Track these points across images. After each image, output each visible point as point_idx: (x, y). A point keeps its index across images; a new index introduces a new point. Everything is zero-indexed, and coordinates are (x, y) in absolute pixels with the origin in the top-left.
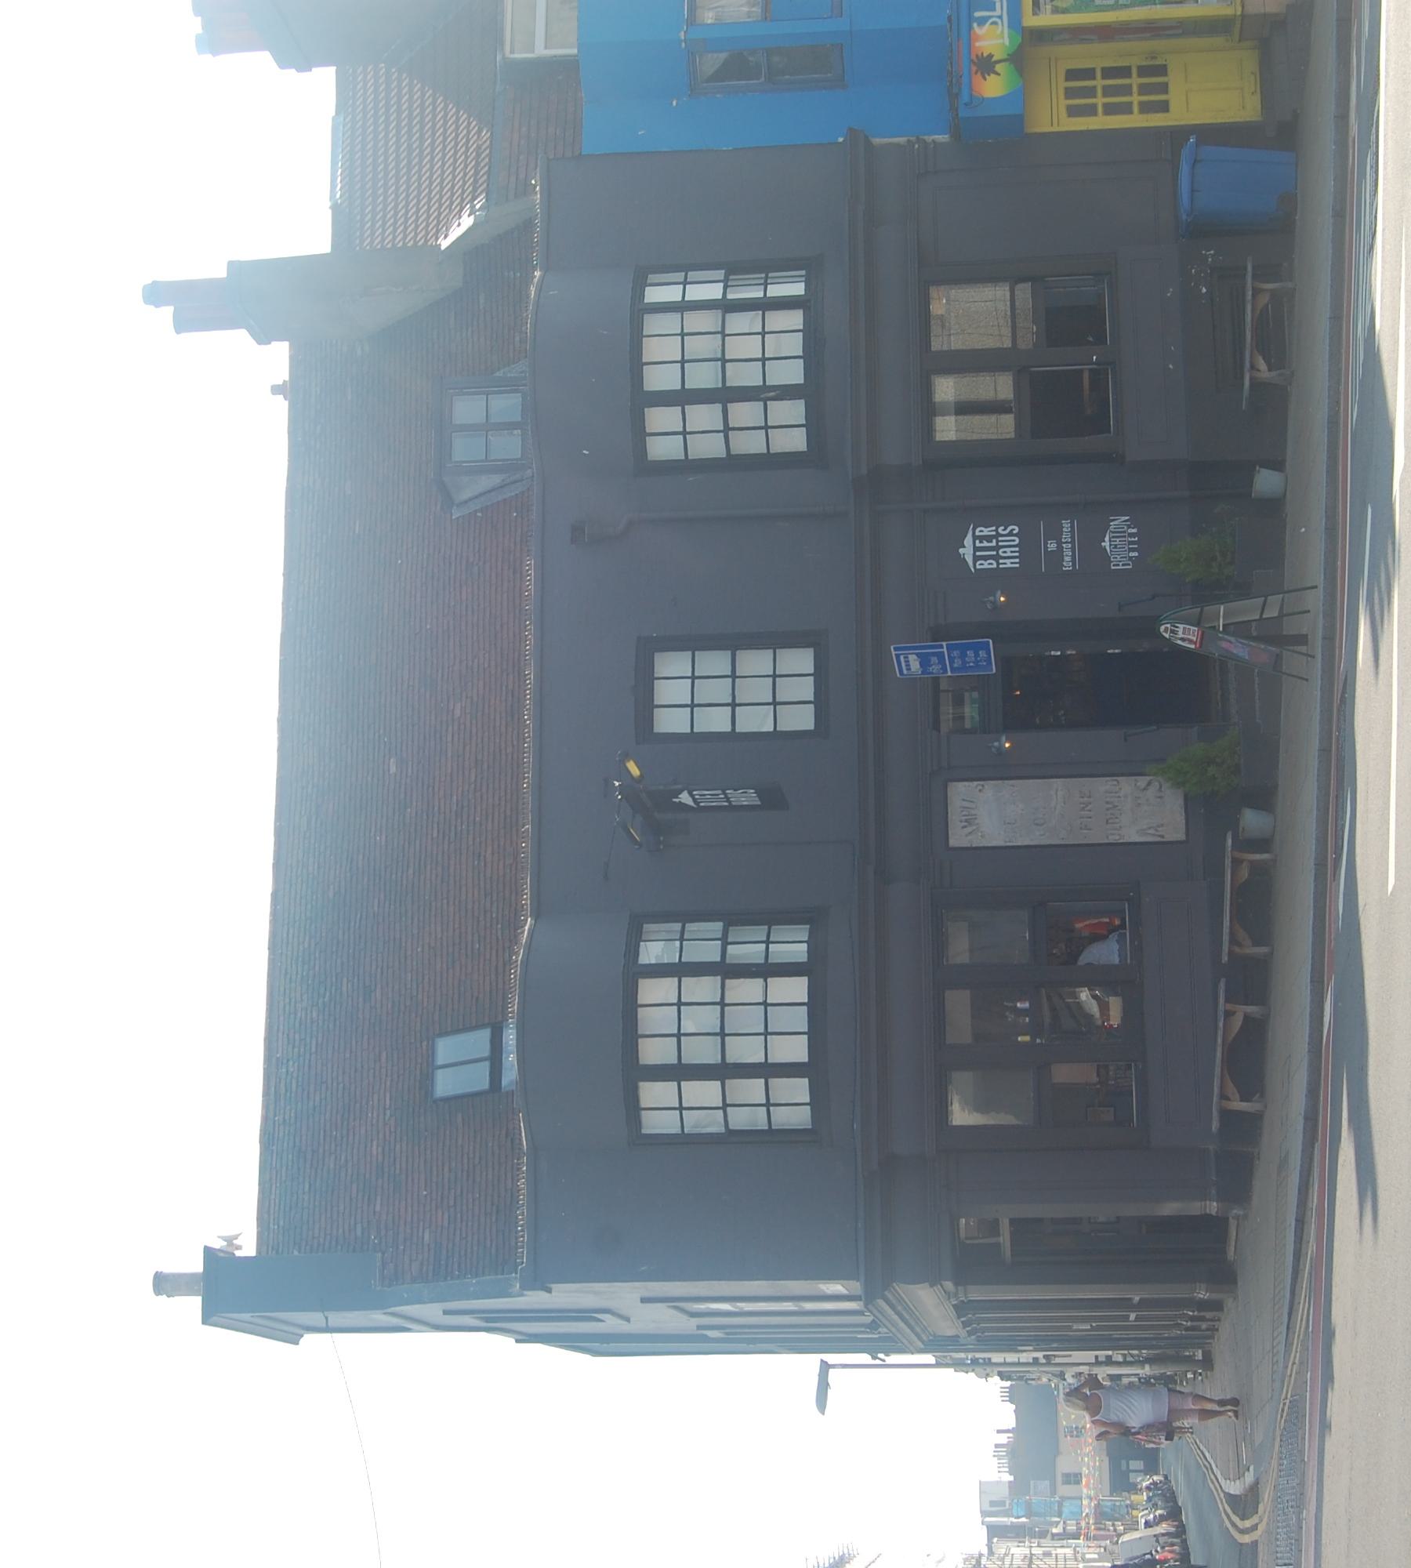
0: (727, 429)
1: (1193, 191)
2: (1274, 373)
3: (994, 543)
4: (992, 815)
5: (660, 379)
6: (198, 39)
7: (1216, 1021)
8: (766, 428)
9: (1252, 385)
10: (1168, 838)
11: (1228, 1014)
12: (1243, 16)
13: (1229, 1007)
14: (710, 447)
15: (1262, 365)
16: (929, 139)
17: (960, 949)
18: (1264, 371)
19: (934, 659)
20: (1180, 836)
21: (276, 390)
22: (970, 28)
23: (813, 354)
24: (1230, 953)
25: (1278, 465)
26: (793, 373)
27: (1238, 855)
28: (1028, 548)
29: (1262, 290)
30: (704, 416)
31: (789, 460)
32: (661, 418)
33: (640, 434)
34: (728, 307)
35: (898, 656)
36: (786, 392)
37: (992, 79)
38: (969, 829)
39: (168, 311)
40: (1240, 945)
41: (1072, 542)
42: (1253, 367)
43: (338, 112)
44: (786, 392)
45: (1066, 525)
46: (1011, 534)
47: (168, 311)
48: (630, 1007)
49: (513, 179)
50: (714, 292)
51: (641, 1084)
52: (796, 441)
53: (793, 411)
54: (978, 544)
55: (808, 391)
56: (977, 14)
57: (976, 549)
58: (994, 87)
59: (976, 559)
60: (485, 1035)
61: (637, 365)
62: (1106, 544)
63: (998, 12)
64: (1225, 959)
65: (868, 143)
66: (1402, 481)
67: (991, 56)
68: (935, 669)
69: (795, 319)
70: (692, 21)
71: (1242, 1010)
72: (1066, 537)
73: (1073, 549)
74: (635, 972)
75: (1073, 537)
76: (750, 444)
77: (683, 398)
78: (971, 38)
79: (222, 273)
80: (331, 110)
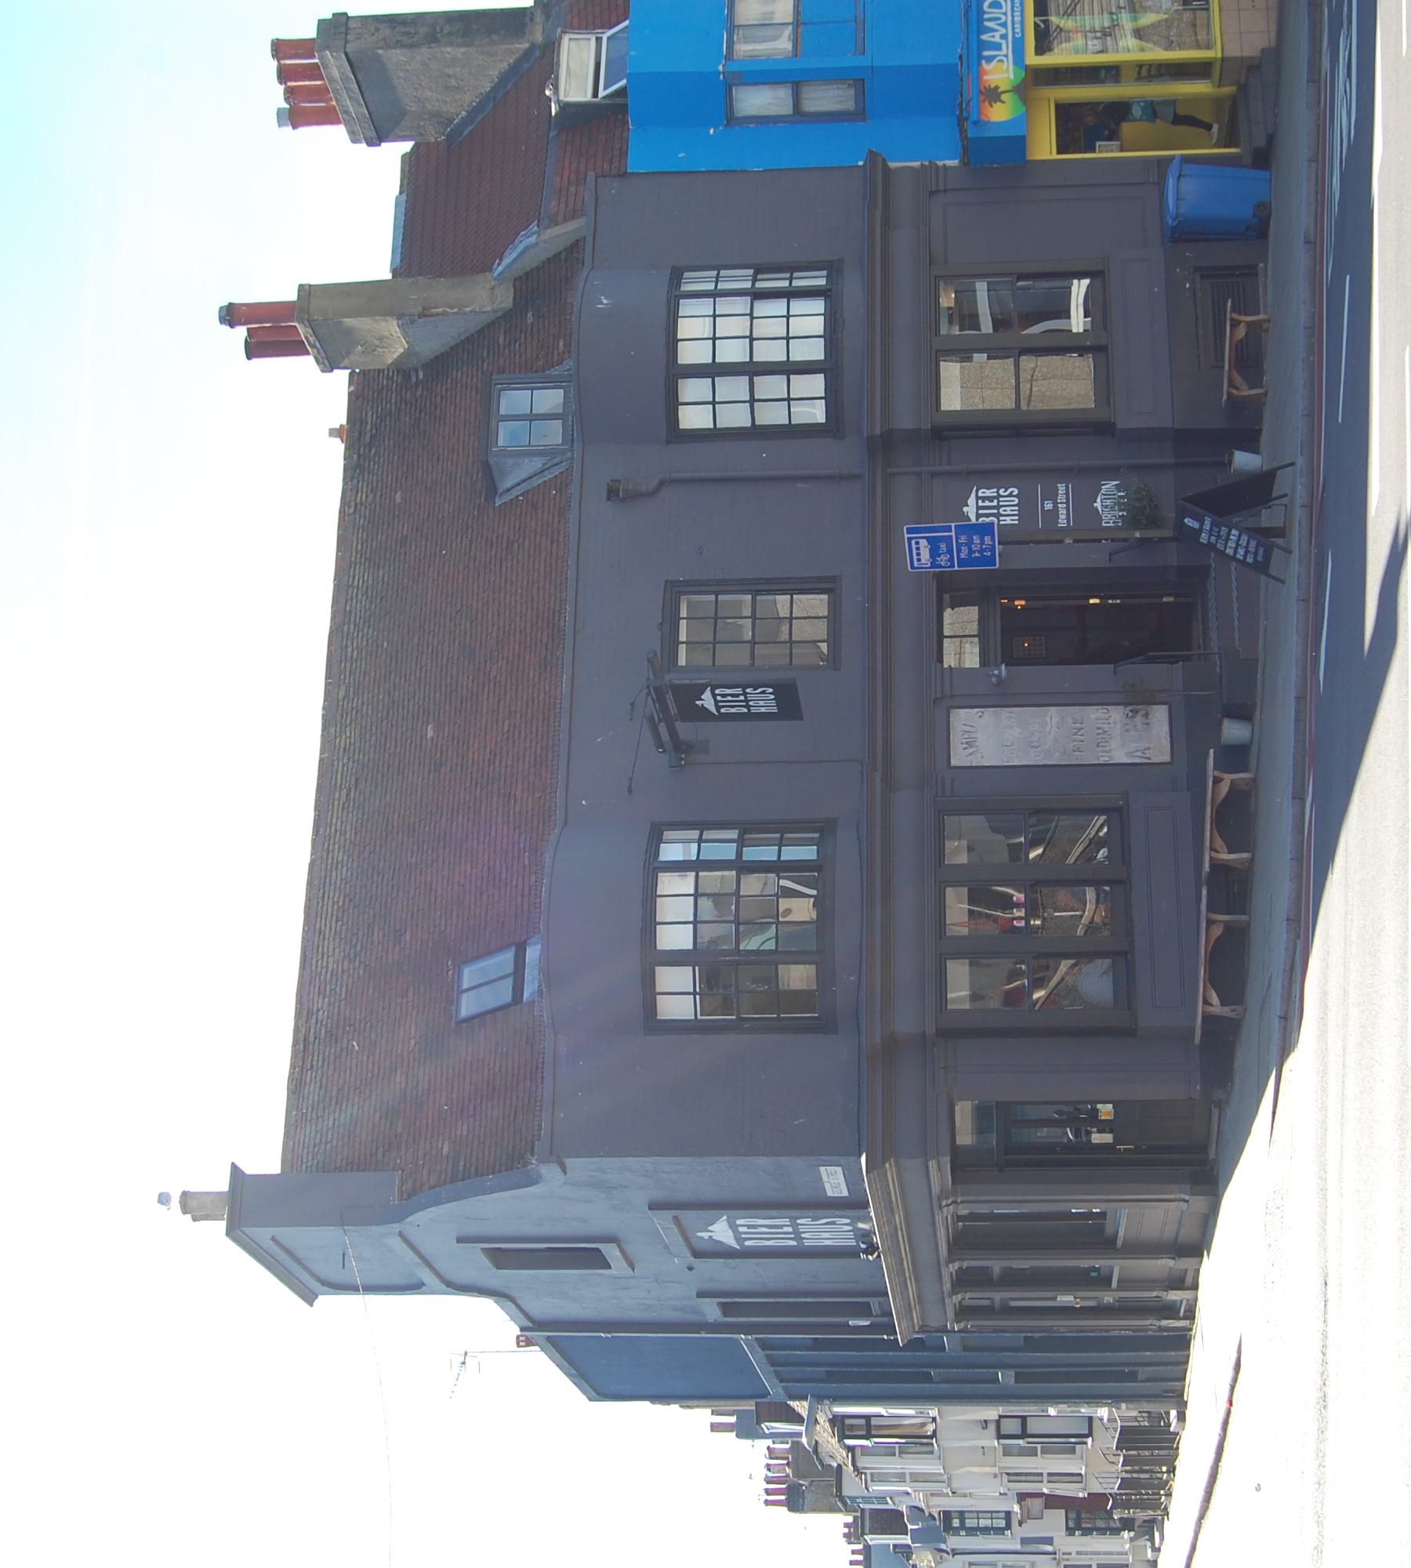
0: (752, 401)
1: (1178, 199)
2: (1226, 1008)
3: (995, 503)
4: (990, 738)
5: (691, 354)
6: (280, 112)
7: (1198, 922)
8: (789, 399)
9: (1212, 866)
10: (1154, 760)
11: (1217, 781)
12: (1223, 59)
13: (1217, 773)
14: (736, 417)
15: (1214, 998)
16: (940, 163)
17: (957, 853)
18: (1216, 1007)
19: (943, 546)
20: (1165, 757)
21: (333, 433)
22: (979, 64)
23: (832, 335)
24: (1229, 393)
25: (1244, 714)
26: (815, 351)
27: (1235, 316)
28: (1026, 506)
29: (1239, 323)
30: (734, 388)
31: (809, 431)
32: (692, 389)
33: (673, 404)
34: (758, 295)
35: (910, 539)
36: (806, 368)
37: (998, 106)
38: (970, 751)
39: (241, 332)
40: (1237, 388)
41: (1067, 503)
42: (1206, 1002)
43: (401, 193)
44: (806, 368)
45: (1061, 488)
46: (1011, 495)
47: (241, 332)
48: (650, 898)
49: (563, 206)
50: (728, 852)
51: (658, 969)
52: (817, 413)
53: (815, 384)
54: (980, 503)
55: (828, 367)
56: (985, 53)
57: (978, 508)
58: (1001, 113)
59: (978, 516)
60: (508, 956)
61: (672, 342)
62: (1098, 505)
63: (1004, 52)
64: (1207, 867)
65: (886, 170)
66: (1381, 170)
67: (997, 88)
68: (943, 560)
69: (818, 306)
70: (729, 56)
71: (1228, 778)
72: (1061, 498)
73: (1068, 508)
74: (654, 867)
75: (1067, 499)
76: (772, 415)
77: (713, 371)
78: (980, 73)
79: (293, 296)
80: (395, 189)
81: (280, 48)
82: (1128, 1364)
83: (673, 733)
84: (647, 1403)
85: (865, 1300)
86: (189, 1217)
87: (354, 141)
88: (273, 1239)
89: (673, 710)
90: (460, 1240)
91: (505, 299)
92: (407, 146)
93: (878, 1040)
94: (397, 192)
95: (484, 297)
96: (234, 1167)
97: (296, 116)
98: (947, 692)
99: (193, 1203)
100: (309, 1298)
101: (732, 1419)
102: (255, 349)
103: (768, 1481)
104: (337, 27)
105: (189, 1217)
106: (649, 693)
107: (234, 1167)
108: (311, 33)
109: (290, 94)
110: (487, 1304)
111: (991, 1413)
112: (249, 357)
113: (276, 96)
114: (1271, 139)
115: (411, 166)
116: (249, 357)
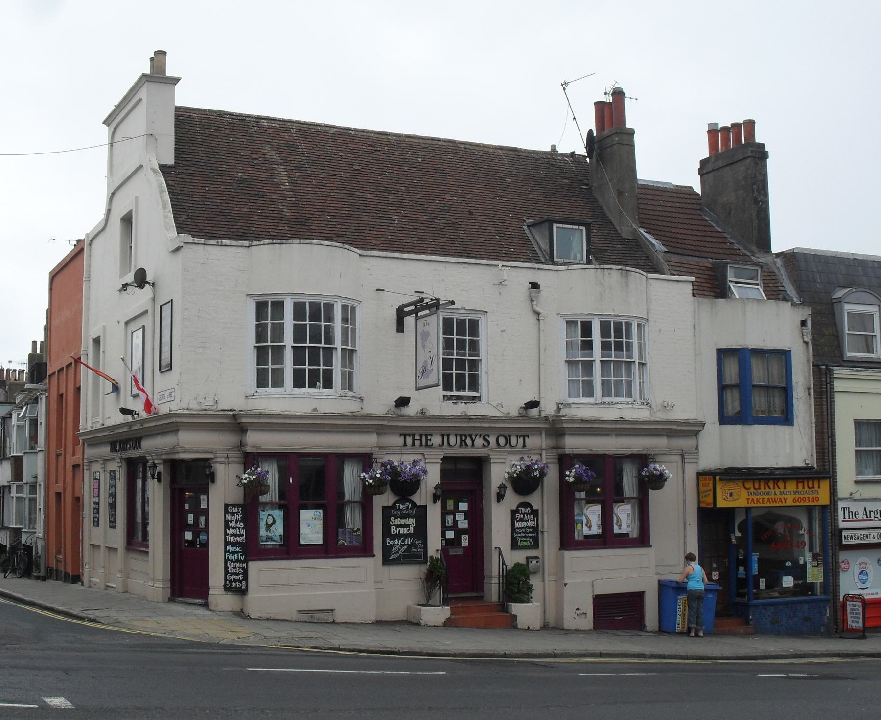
6: (716, 124)
21: (554, 147)
39: (609, 99)
47: (609, 99)
81: (750, 125)
82: (65, 550)
84: (47, 307)
85: (101, 415)
88: (140, 100)
90: (137, 197)
91: (625, 233)
92: (698, 189)
93: (244, 420)
96: (178, 80)
97: (713, 132)
99: (161, 56)
100: (107, 122)
101: (38, 352)
102: (600, 106)
103: (8, 370)
104: (760, 154)
106: (432, 300)
107: (178, 80)
108: (758, 140)
109: (725, 130)
110: (101, 216)
111: (40, 480)
112: (596, 103)
113: (725, 122)
115: (685, 192)
116: (596, 103)
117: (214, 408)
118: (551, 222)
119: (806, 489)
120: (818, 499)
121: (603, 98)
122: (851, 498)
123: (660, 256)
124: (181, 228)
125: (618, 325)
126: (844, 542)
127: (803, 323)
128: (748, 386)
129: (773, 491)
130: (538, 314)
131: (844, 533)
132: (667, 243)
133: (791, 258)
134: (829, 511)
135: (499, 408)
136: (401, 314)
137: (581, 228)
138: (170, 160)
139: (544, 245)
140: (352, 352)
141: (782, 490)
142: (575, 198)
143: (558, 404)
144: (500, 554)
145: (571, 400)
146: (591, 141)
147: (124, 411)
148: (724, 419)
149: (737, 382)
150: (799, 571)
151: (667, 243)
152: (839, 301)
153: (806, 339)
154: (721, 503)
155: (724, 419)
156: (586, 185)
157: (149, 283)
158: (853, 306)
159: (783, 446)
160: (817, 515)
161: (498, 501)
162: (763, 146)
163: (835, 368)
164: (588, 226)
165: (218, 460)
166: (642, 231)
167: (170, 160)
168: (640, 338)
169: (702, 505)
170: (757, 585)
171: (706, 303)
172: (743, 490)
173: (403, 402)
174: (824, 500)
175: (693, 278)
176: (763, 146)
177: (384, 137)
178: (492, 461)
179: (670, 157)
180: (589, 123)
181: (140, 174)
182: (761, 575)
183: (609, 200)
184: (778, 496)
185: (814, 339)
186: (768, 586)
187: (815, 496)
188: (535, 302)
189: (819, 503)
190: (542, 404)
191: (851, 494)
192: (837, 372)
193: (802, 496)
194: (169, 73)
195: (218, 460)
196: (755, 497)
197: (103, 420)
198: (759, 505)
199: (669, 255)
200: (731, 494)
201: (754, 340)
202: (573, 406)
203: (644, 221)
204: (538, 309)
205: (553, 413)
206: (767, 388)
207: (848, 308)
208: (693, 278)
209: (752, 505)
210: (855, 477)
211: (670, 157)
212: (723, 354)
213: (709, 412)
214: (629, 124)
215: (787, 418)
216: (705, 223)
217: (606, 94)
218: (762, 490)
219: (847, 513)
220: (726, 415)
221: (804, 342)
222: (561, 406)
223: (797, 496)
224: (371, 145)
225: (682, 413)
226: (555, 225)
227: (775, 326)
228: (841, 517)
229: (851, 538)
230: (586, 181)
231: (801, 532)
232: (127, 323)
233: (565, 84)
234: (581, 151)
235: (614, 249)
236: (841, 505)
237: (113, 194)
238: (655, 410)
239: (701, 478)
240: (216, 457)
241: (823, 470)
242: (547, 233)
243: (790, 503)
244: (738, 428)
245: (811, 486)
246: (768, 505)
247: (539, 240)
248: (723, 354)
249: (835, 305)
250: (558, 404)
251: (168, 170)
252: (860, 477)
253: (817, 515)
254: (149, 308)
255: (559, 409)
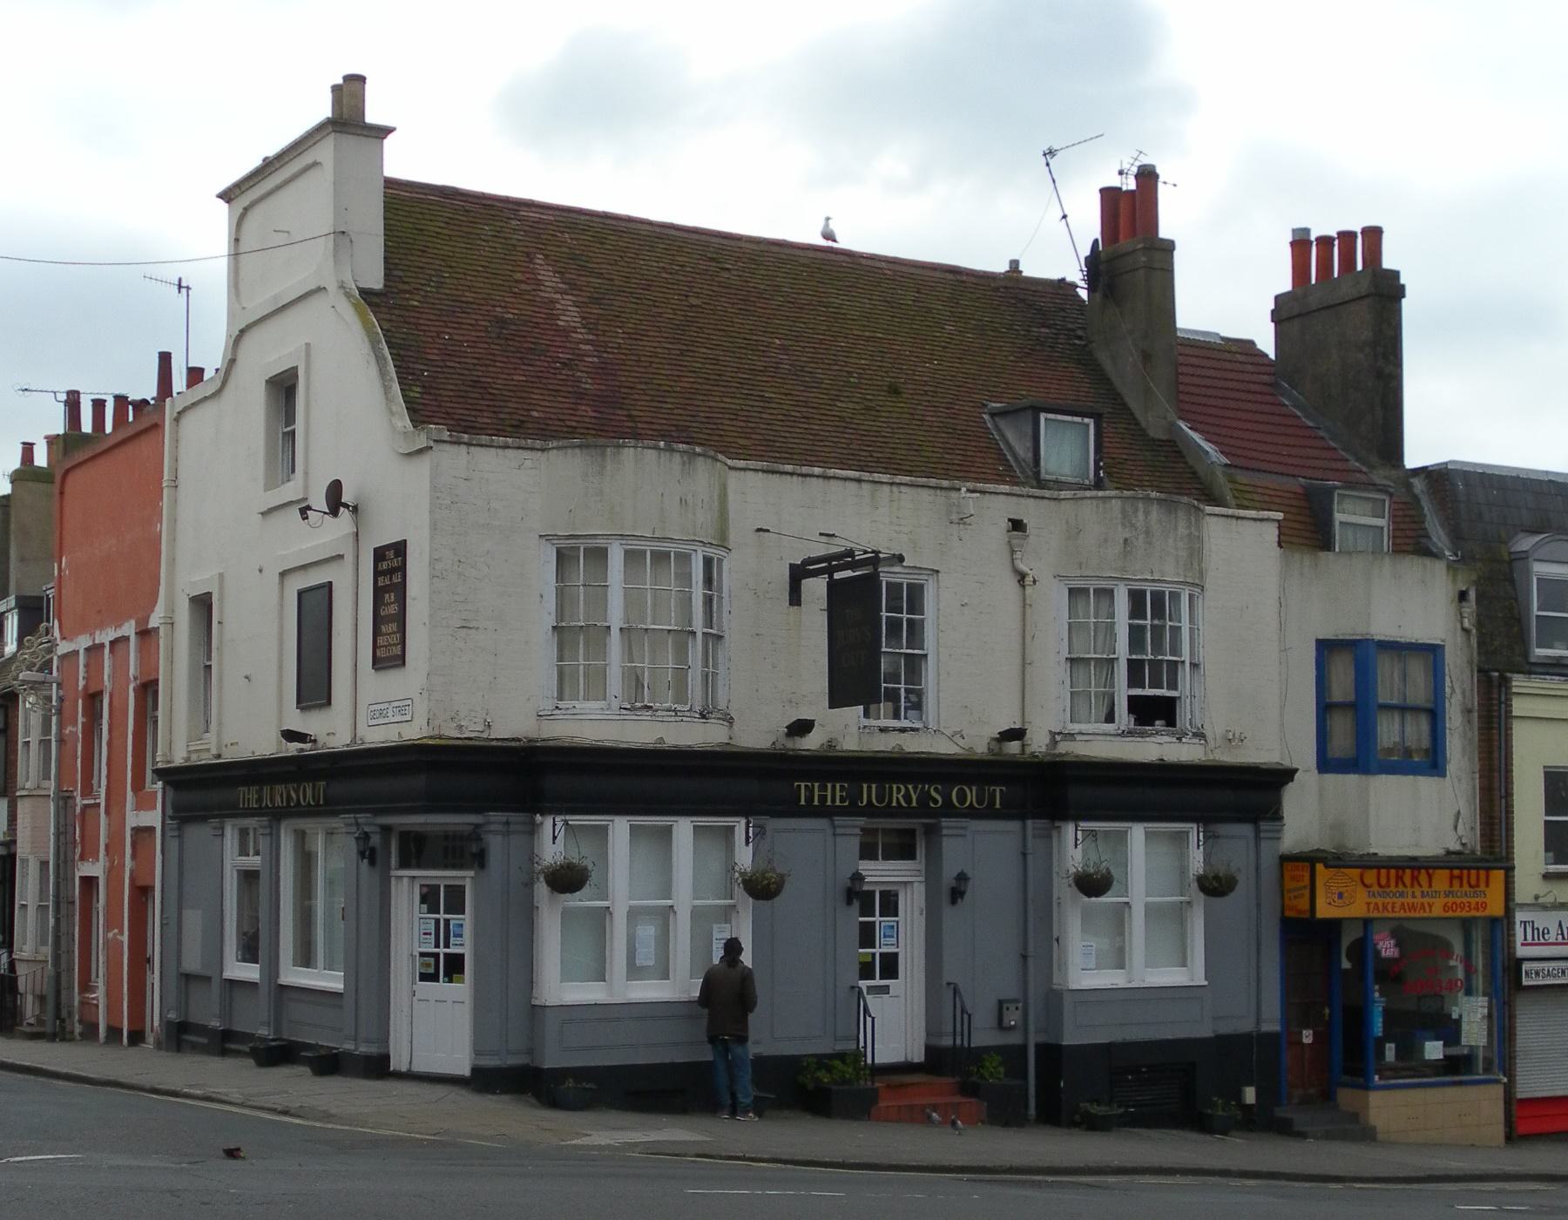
6: (1307, 231)
21: (1015, 264)
39: (1131, 184)
43: (1223, 339)
47: (1131, 184)
81: (1373, 235)
83: (815, 573)
86: (340, 81)
87: (1277, 298)
88: (315, 164)
89: (837, 576)
90: (308, 345)
91: (1157, 432)
94: (1223, 334)
95: (1158, 417)
98: (839, 831)
102: (1110, 197)
105: (340, 81)
106: (866, 552)
108: (1388, 263)
109: (1325, 242)
114: (1302, 1135)
117: (485, 735)
118: (1036, 410)
119: (1466, 887)
120: (1484, 906)
121: (1115, 181)
122: (1537, 905)
123: (1221, 478)
124: (419, 414)
125: (1158, 598)
126: (1525, 982)
127: (1463, 596)
128: (1359, 705)
129: (1410, 890)
130: (1022, 577)
131: (1526, 966)
132: (1226, 449)
133: (1440, 478)
134: (1500, 927)
135: (957, 738)
136: (798, 574)
137: (1086, 420)
138: (376, 281)
139: (1022, 449)
140: (720, 638)
141: (1425, 889)
142: (1066, 366)
143: (1053, 734)
144: (956, 991)
145: (1076, 727)
146: (1095, 265)
147: (290, 736)
148: (1326, 764)
149: (1351, 698)
150: (1449, 1030)
151: (1226, 449)
152: (1524, 557)
153: (1466, 624)
154: (1324, 910)
155: (1326, 764)
156: (1080, 338)
157: (346, 506)
158: (1550, 566)
159: (1413, 816)
160: (1478, 936)
161: (954, 902)
162: (1396, 274)
163: (1515, 676)
164: (1097, 417)
165: (492, 827)
166: (1182, 425)
167: (376, 281)
168: (1191, 621)
169: (1288, 914)
170: (1381, 1053)
171: (1303, 561)
172: (1360, 888)
173: (801, 728)
174: (1496, 909)
175: (1280, 516)
176: (1396, 274)
177: (732, 243)
178: (945, 832)
179: (1227, 291)
180: (1089, 226)
181: (316, 303)
182: (1387, 1037)
183: (1123, 367)
184: (1419, 900)
185: (1480, 624)
186: (1399, 1054)
187: (1479, 900)
188: (1018, 555)
189: (1487, 913)
190: (1028, 735)
191: (1537, 897)
192: (1519, 682)
193: (1458, 901)
194: (370, 118)
195: (492, 827)
196: (1380, 901)
197: (219, 747)
198: (1386, 915)
199: (1233, 471)
200: (1340, 896)
201: (1383, 627)
202: (1079, 738)
203: (1187, 407)
204: (1023, 567)
205: (1043, 749)
206: (1403, 709)
207: (1540, 569)
208: (1280, 516)
209: (1375, 915)
210: (1543, 869)
211: (1227, 291)
212: (1326, 649)
213: (1303, 755)
214: (1164, 232)
215: (1433, 763)
216: (1284, 410)
217: (1121, 173)
218: (1393, 888)
219: (1529, 930)
220: (1330, 755)
221: (1464, 629)
222: (1058, 738)
223: (1451, 899)
224: (712, 259)
225: (1261, 752)
226: (1043, 416)
227: (1417, 605)
228: (1519, 938)
229: (1537, 974)
230: (1080, 333)
231: (1452, 963)
232: (283, 574)
233: (1051, 153)
234: (1074, 273)
235: (1145, 464)
236: (1520, 916)
237: (242, 332)
238: (1212, 744)
239: (1288, 866)
240: (490, 823)
241: (1492, 850)
242: (1029, 430)
243: (1437, 911)
244: (1352, 778)
245: (1473, 882)
246: (1402, 914)
247: (1014, 438)
248: (1326, 649)
249: (1517, 565)
250: (1053, 734)
251: (376, 300)
252: (1553, 868)
253: (1478, 936)
254: (347, 550)
255: (1054, 743)
